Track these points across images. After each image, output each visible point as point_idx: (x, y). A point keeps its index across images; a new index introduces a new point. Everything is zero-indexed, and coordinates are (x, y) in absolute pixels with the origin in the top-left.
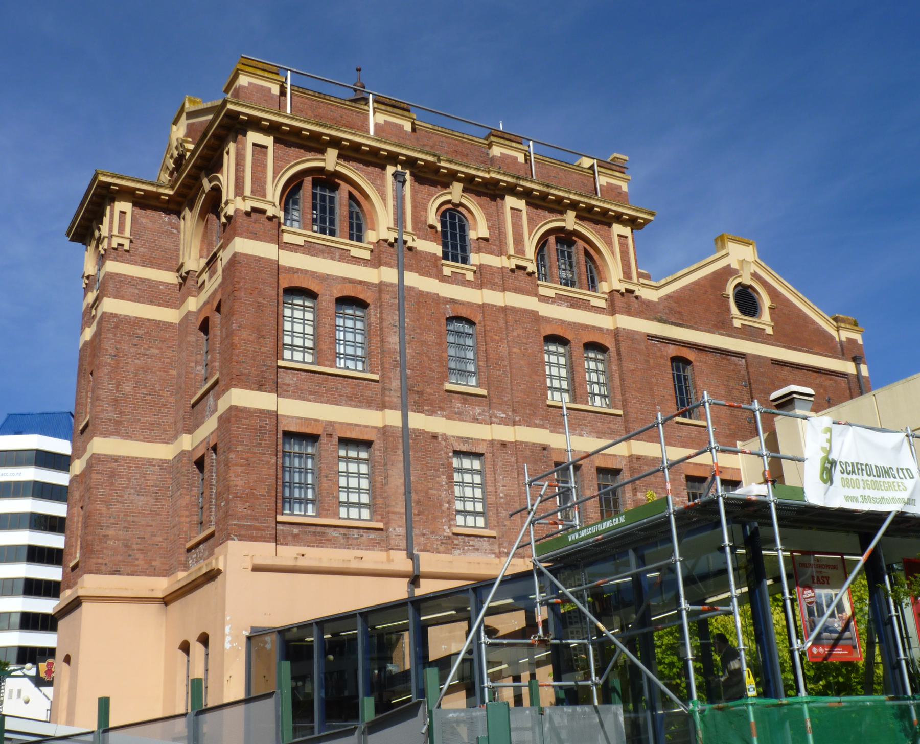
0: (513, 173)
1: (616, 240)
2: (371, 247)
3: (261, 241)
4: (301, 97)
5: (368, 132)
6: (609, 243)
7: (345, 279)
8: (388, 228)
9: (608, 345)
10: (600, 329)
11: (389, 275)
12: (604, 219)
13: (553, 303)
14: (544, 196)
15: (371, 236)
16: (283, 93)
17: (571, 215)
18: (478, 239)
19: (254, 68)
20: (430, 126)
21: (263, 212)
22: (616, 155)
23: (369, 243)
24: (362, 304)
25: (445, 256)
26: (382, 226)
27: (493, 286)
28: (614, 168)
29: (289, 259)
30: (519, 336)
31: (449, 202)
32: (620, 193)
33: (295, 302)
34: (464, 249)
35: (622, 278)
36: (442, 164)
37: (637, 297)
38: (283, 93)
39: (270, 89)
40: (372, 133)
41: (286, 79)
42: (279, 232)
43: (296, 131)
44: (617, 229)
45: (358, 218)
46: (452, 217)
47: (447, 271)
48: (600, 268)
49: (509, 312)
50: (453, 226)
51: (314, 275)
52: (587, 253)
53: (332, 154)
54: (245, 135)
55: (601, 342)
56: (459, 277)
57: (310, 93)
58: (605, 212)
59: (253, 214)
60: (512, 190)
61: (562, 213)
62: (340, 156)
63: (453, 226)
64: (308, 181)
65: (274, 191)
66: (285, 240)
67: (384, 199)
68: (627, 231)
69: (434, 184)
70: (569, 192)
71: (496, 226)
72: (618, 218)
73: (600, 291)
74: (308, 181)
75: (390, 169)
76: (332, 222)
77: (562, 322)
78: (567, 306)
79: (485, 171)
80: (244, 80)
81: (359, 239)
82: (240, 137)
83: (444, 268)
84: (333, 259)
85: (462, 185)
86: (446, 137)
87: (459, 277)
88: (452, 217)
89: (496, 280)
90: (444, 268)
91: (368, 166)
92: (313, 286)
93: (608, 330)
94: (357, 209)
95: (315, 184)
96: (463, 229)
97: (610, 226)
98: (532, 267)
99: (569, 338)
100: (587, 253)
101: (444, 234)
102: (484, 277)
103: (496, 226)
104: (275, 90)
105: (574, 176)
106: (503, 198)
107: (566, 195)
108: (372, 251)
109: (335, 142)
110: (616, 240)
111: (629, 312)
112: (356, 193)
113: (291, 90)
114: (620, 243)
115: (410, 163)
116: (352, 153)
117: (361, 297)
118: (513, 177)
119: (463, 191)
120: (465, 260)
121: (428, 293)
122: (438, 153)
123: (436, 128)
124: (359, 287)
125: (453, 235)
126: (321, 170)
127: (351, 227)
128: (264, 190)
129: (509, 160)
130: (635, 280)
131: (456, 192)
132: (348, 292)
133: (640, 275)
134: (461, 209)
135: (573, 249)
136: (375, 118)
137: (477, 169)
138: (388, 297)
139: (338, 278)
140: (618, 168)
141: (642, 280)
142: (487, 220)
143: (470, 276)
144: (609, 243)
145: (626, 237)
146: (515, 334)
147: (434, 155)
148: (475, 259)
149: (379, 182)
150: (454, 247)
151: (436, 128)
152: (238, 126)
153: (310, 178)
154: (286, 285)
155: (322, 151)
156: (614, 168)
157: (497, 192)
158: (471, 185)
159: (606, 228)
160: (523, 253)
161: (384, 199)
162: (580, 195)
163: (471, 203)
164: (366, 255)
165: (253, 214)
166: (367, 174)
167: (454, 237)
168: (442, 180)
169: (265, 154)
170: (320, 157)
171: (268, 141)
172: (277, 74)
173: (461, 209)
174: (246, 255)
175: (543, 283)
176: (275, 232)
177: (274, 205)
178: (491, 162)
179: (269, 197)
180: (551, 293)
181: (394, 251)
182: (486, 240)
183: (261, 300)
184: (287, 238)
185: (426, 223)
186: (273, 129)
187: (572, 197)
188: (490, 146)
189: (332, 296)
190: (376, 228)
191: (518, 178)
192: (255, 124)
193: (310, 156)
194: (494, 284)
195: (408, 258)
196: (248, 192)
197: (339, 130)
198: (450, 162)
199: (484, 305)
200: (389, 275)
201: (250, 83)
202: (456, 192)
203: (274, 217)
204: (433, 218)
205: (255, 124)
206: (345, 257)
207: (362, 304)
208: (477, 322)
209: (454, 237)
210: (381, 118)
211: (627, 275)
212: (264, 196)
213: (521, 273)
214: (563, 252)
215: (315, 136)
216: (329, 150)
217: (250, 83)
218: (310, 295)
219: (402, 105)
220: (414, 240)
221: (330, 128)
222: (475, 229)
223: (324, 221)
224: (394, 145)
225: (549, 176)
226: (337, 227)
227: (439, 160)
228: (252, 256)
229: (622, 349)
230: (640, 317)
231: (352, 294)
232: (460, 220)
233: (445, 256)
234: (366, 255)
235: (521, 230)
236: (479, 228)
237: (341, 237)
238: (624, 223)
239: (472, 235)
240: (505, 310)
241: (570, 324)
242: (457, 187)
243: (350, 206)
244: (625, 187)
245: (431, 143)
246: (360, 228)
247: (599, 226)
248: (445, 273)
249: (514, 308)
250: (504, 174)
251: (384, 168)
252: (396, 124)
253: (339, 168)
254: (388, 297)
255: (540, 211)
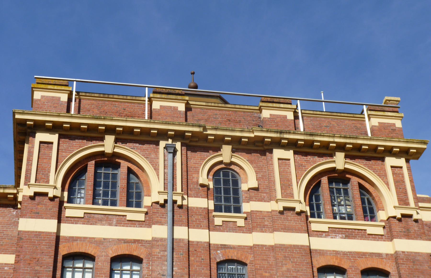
0: (275, 129)
1: (389, 171)
2: (383, 224)
3: (42, 218)
4: (89, 99)
5: (367, 134)
6: (383, 176)
7: (120, 240)
8: (395, 207)
9: (388, 269)
10: (379, 255)
11: (160, 231)
12: (375, 155)
13: (326, 236)
14: (310, 144)
15: (382, 215)
16: (296, 117)
17: (340, 156)
18: (249, 189)
19: (45, 84)
20: (204, 104)
21: (293, 209)
22: (387, 98)
23: (382, 221)
24: (138, 260)
25: (218, 208)
26: (155, 190)
27: (263, 228)
28: (387, 109)
29: (317, 244)
30: (288, 270)
31: (221, 162)
32: (394, 130)
33: (77, 265)
34: (237, 200)
35: (397, 205)
36: (209, 132)
37: (416, 221)
38: (296, 117)
39: (285, 117)
40: (370, 135)
41: (297, 106)
42: (308, 223)
43: (75, 127)
44: (390, 161)
45: (370, 203)
46: (226, 175)
47: (218, 221)
48: (377, 199)
49: (278, 249)
50: (226, 182)
51: (91, 240)
52: (361, 187)
53: (110, 139)
54: (34, 137)
55: (381, 266)
56: (231, 225)
57: (96, 95)
58: (374, 148)
59: (285, 212)
60: (278, 144)
61: (331, 155)
62: (346, 157)
63: (226, 182)
64: (324, 180)
65: (299, 192)
66: (313, 229)
67: (156, 169)
68: (401, 162)
69: (206, 149)
70: (334, 137)
71: (265, 176)
72: (390, 152)
73: (379, 220)
74: (324, 180)
75: (163, 144)
76: (114, 194)
77: (336, 253)
78: (342, 238)
79: (249, 132)
80: (37, 95)
81: (373, 218)
82: (31, 139)
83: (216, 219)
84: (110, 225)
85: (231, 147)
86: (219, 110)
87: (231, 225)
88: (226, 175)
89: (266, 223)
90: (216, 219)
91: (143, 144)
92: (90, 251)
93: (387, 255)
94: (368, 196)
95: (330, 181)
96: (236, 183)
97: (383, 160)
98: (303, 207)
99: (345, 267)
100: (361, 187)
101: (217, 190)
102: (255, 223)
103: (265, 176)
104: (290, 116)
105: (347, 122)
106: (271, 152)
107: (331, 140)
108: (384, 227)
109: (110, 130)
110: (389, 171)
111: (408, 235)
112: (367, 185)
113: (302, 113)
114: (393, 174)
115: (179, 136)
116: (355, 153)
117: (135, 253)
118: (277, 132)
119: (233, 151)
120: (238, 210)
121: (198, 242)
122: (202, 123)
123: (210, 104)
124: (134, 245)
125: (226, 191)
126: (333, 170)
127: (365, 211)
128: (48, 177)
129: (279, 119)
130: (412, 204)
131: (226, 153)
132: (124, 250)
133: (417, 200)
134: (232, 167)
135: (349, 185)
136: (371, 123)
137: (242, 131)
138: (158, 250)
139: (113, 240)
140: (391, 109)
141: (421, 205)
142: (257, 172)
143: (241, 223)
144: (383, 176)
145: (401, 167)
146: (284, 268)
147: (200, 126)
148: (246, 207)
149: (153, 156)
150: (227, 200)
151: (210, 104)
152: (29, 131)
153: (93, 162)
154: (318, 266)
155: (102, 139)
156: (387, 109)
157: (266, 147)
158: (238, 145)
159: (379, 162)
160: (292, 195)
161: (156, 169)
162: (345, 137)
163: (241, 160)
164: (380, 231)
165: (285, 212)
166: (370, 168)
167: (227, 191)
168: (214, 145)
169: (51, 149)
170: (101, 143)
171: (289, 154)
172: (291, 104)
173: (232, 167)
174: (28, 232)
175: (316, 219)
176: (304, 224)
177: (300, 202)
178: (260, 124)
179: (296, 198)
180: (325, 228)
181: (174, 212)
182: (256, 189)
183: (37, 268)
184: (314, 227)
185: (198, 183)
186: (56, 128)
187: (337, 140)
188: (260, 110)
189: (107, 256)
190: (385, 209)
191: (281, 132)
192: (40, 126)
193: (323, 160)
194: (264, 226)
195: (180, 215)
196: (33, 181)
197: (112, 120)
198: (216, 129)
199: (255, 246)
200: (160, 231)
201: (42, 97)
202: (226, 153)
203: (302, 212)
204: (203, 178)
205: (40, 126)
206: (122, 221)
207: (138, 260)
208: (248, 262)
209: (227, 191)
210: (375, 122)
211: (403, 201)
212: (293, 197)
213: (290, 213)
214: (338, 190)
215: (92, 128)
216: (107, 137)
217: (161, 106)
218: (90, 258)
219: (177, 92)
220: (418, 213)
221: (105, 119)
222: (246, 182)
223: (103, 193)
224: (162, 123)
225: (321, 127)
226: (118, 198)
227: (205, 129)
228: (33, 232)
229: (402, 272)
230: (421, 239)
231: (127, 253)
232: (233, 176)
233: (218, 208)
234: (380, 231)
235: (288, 177)
236: (249, 180)
237: (357, 220)
238: (397, 155)
239: (244, 187)
240: (273, 248)
241: (345, 254)
242: (226, 150)
243: (361, 194)
244: (398, 124)
245: (206, 117)
246: (372, 211)
247: (372, 162)
248: (216, 223)
249: (284, 245)
250: (267, 131)
251: (157, 144)
252: (171, 107)
253: (347, 166)
254: (158, 250)
255: (309, 157)
